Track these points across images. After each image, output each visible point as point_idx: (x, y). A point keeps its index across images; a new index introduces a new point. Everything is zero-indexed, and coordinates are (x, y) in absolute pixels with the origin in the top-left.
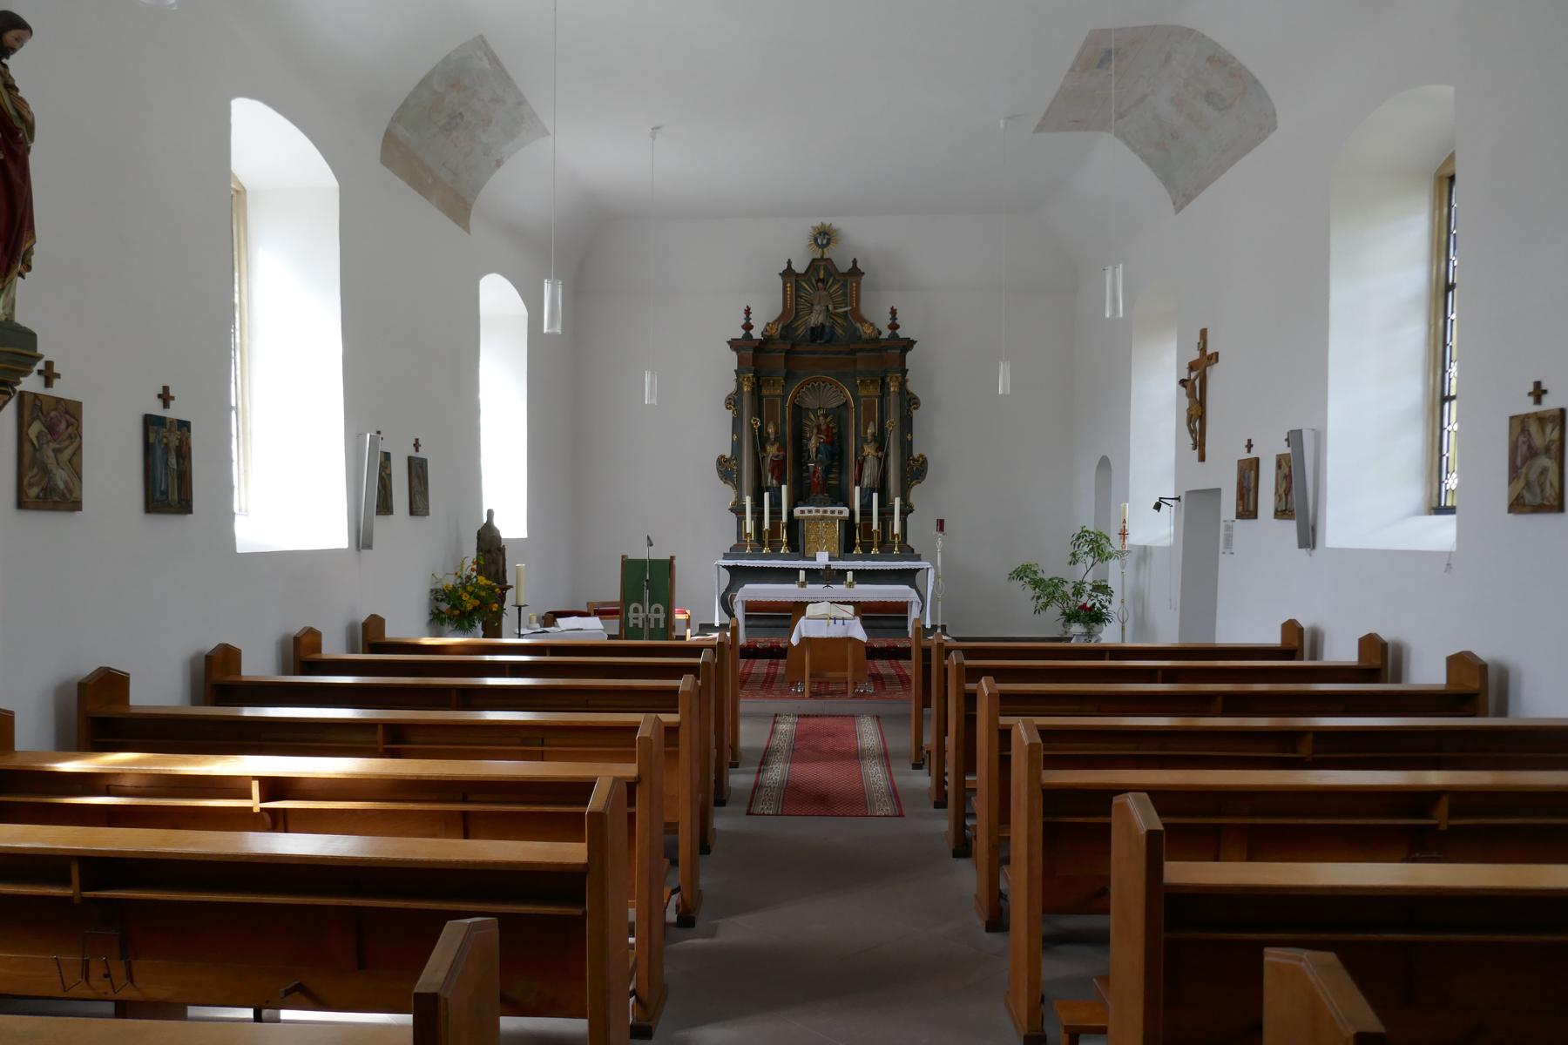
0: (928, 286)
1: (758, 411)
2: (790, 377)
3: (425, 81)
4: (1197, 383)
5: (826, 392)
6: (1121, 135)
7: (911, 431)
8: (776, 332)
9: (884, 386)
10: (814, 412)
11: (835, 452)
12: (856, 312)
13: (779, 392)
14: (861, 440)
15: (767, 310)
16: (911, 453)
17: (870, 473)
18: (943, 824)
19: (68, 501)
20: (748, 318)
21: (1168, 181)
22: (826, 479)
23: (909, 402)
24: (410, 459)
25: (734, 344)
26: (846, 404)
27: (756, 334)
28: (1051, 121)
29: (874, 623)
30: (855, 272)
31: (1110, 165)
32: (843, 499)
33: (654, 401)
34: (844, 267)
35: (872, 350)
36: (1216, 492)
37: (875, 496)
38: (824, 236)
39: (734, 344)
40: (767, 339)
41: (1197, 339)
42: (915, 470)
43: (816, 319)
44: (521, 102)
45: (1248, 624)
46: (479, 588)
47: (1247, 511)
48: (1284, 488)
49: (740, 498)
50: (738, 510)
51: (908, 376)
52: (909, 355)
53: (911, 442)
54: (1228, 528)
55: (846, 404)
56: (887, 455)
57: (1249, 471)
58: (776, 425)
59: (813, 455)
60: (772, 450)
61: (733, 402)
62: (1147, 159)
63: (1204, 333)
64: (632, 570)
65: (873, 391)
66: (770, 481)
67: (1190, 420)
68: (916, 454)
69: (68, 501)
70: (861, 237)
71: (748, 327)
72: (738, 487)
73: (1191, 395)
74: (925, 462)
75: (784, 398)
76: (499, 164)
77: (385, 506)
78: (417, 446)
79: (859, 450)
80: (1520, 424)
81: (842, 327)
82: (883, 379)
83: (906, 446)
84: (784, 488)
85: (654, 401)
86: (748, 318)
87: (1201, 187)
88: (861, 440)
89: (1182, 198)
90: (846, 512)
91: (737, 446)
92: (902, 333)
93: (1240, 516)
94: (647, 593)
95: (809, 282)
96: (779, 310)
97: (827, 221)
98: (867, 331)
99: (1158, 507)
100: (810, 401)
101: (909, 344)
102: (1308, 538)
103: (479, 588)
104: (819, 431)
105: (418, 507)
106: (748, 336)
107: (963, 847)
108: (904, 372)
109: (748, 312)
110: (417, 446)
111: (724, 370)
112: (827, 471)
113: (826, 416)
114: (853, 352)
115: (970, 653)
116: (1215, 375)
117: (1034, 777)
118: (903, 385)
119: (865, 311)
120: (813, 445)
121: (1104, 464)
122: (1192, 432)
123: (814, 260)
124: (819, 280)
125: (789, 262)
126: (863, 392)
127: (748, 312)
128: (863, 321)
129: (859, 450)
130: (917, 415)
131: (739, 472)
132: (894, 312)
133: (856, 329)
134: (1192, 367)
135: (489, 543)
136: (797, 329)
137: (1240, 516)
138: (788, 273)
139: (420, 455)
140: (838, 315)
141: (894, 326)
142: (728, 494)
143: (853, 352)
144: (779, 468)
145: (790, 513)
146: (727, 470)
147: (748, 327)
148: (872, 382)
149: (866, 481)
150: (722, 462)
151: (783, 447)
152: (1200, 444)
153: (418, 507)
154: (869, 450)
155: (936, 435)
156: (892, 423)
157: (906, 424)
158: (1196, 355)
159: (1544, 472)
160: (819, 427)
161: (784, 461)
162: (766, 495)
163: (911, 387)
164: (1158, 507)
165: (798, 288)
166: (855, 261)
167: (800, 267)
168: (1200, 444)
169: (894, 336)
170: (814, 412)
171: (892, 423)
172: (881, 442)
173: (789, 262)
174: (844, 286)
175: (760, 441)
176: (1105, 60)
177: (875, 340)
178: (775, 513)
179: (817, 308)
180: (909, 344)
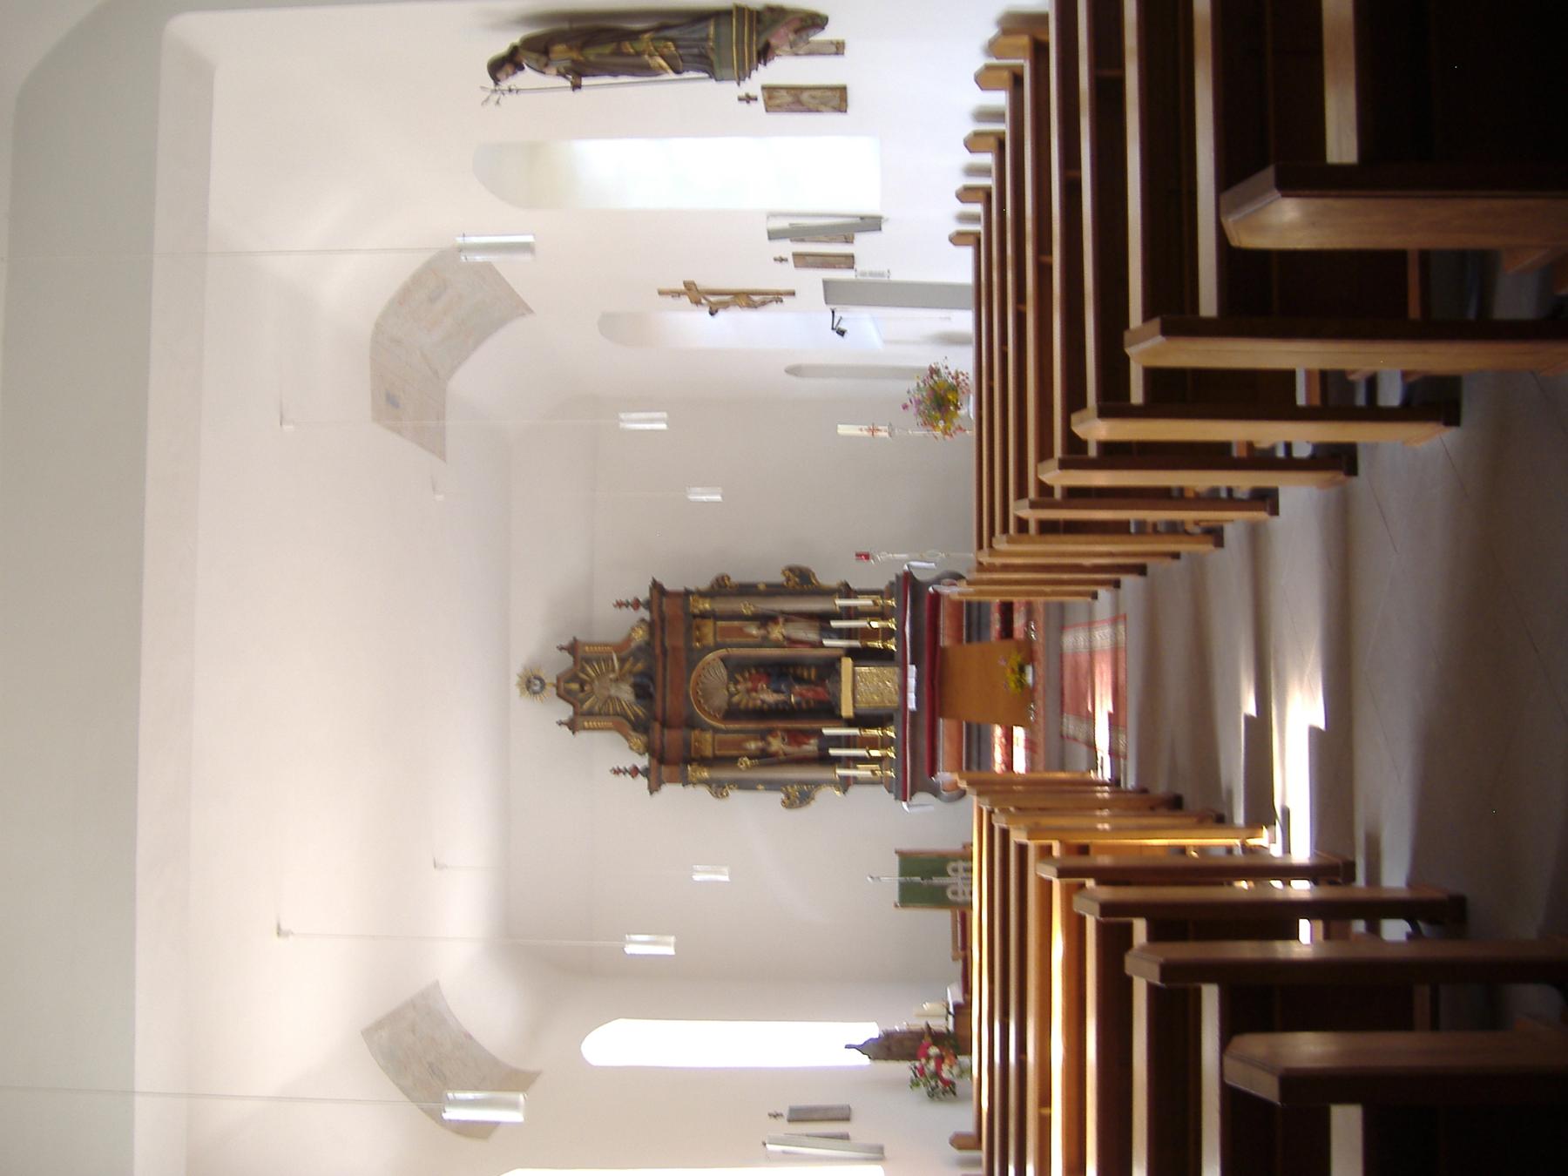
0: (592, 572)
1: (731, 761)
2: (692, 723)
3: (404, 1090)
4: (713, 299)
5: (705, 682)
6: (454, 369)
7: (754, 586)
8: (639, 740)
9: (704, 615)
10: (731, 695)
11: (779, 671)
12: (618, 648)
13: (708, 736)
14: (765, 642)
15: (616, 749)
16: (780, 586)
17: (806, 633)
18: (1128, 581)
19: (842, 91)
20: (625, 772)
21: (501, 323)
22: (808, 682)
23: (721, 588)
24: (790, 1121)
25: (654, 788)
26: (724, 660)
27: (643, 762)
28: (432, 440)
29: (974, 634)
30: (573, 648)
31: (478, 381)
32: (829, 668)
33: (726, 870)
34: (567, 660)
35: (663, 629)
36: (826, 283)
37: (834, 624)
38: (532, 683)
39: (654, 788)
40: (649, 749)
41: (669, 299)
42: (801, 581)
43: (625, 693)
44: (412, 1004)
45: (960, 268)
46: (924, 1053)
47: (848, 261)
48: (826, 245)
49: (832, 783)
50: (845, 784)
51: (692, 588)
52: (668, 587)
53: (768, 586)
54: (863, 274)
55: (724, 660)
56: (783, 613)
57: (802, 260)
58: (747, 740)
59: (780, 697)
60: (776, 744)
61: (718, 788)
62: (478, 343)
63: (661, 293)
64: (911, 896)
65: (708, 628)
66: (811, 746)
67: (753, 306)
68: (781, 579)
69: (842, 91)
70: (534, 639)
71: (634, 772)
72: (818, 784)
73: (726, 305)
74: (791, 570)
75: (716, 730)
76: (469, 1036)
77: (845, 1137)
78: (776, 1116)
79: (777, 645)
80: (769, 108)
81: (634, 664)
82: (695, 616)
83: (774, 591)
84: (826, 731)
85: (726, 870)
86: (625, 772)
87: (511, 292)
88: (765, 642)
89: (521, 308)
90: (847, 663)
91: (771, 785)
92: (644, 595)
93: (851, 267)
94: (937, 881)
95: (583, 702)
96: (616, 737)
97: (515, 679)
98: (640, 635)
99: (842, 333)
100: (720, 700)
101: (657, 587)
102: (872, 224)
103: (924, 1053)
104: (755, 690)
105: (844, 1116)
106: (646, 773)
107: (1141, 570)
108: (688, 593)
109: (617, 772)
110: (776, 1116)
111: (685, 802)
112: (800, 680)
113: (736, 682)
114: (664, 652)
115: (980, 547)
116: (704, 283)
117: (1032, 541)
118: (702, 595)
119: (617, 636)
120: (770, 697)
121: (794, 371)
122: (764, 303)
123: (559, 695)
124: (582, 690)
125: (560, 723)
126: (710, 640)
127: (617, 772)
128: (629, 639)
129: (777, 645)
130: (736, 578)
131: (801, 783)
132: (620, 605)
133: (639, 648)
134: (698, 303)
135: (887, 1048)
136: (636, 716)
137: (851, 267)
138: (573, 726)
139: (786, 1113)
140: (621, 668)
141: (636, 604)
142: (828, 797)
143: (664, 652)
144: (795, 737)
145: (850, 723)
146: (799, 797)
147: (634, 772)
148: (698, 628)
149: (812, 636)
150: (790, 803)
151: (771, 732)
152: (777, 297)
153: (844, 1116)
154: (777, 632)
155: (761, 562)
156: (746, 606)
157: (747, 590)
158: (685, 300)
159: (814, 97)
160: (748, 691)
161: (788, 731)
162: (833, 752)
163: (704, 584)
164: (842, 333)
165: (590, 714)
166: (561, 648)
167: (566, 711)
168: (777, 297)
169: (648, 605)
170: (731, 695)
171: (746, 606)
172: (766, 619)
173: (560, 723)
174: (588, 661)
175: (765, 758)
176: (392, 401)
177: (651, 626)
178: (848, 742)
179: (613, 692)
180: (657, 587)
